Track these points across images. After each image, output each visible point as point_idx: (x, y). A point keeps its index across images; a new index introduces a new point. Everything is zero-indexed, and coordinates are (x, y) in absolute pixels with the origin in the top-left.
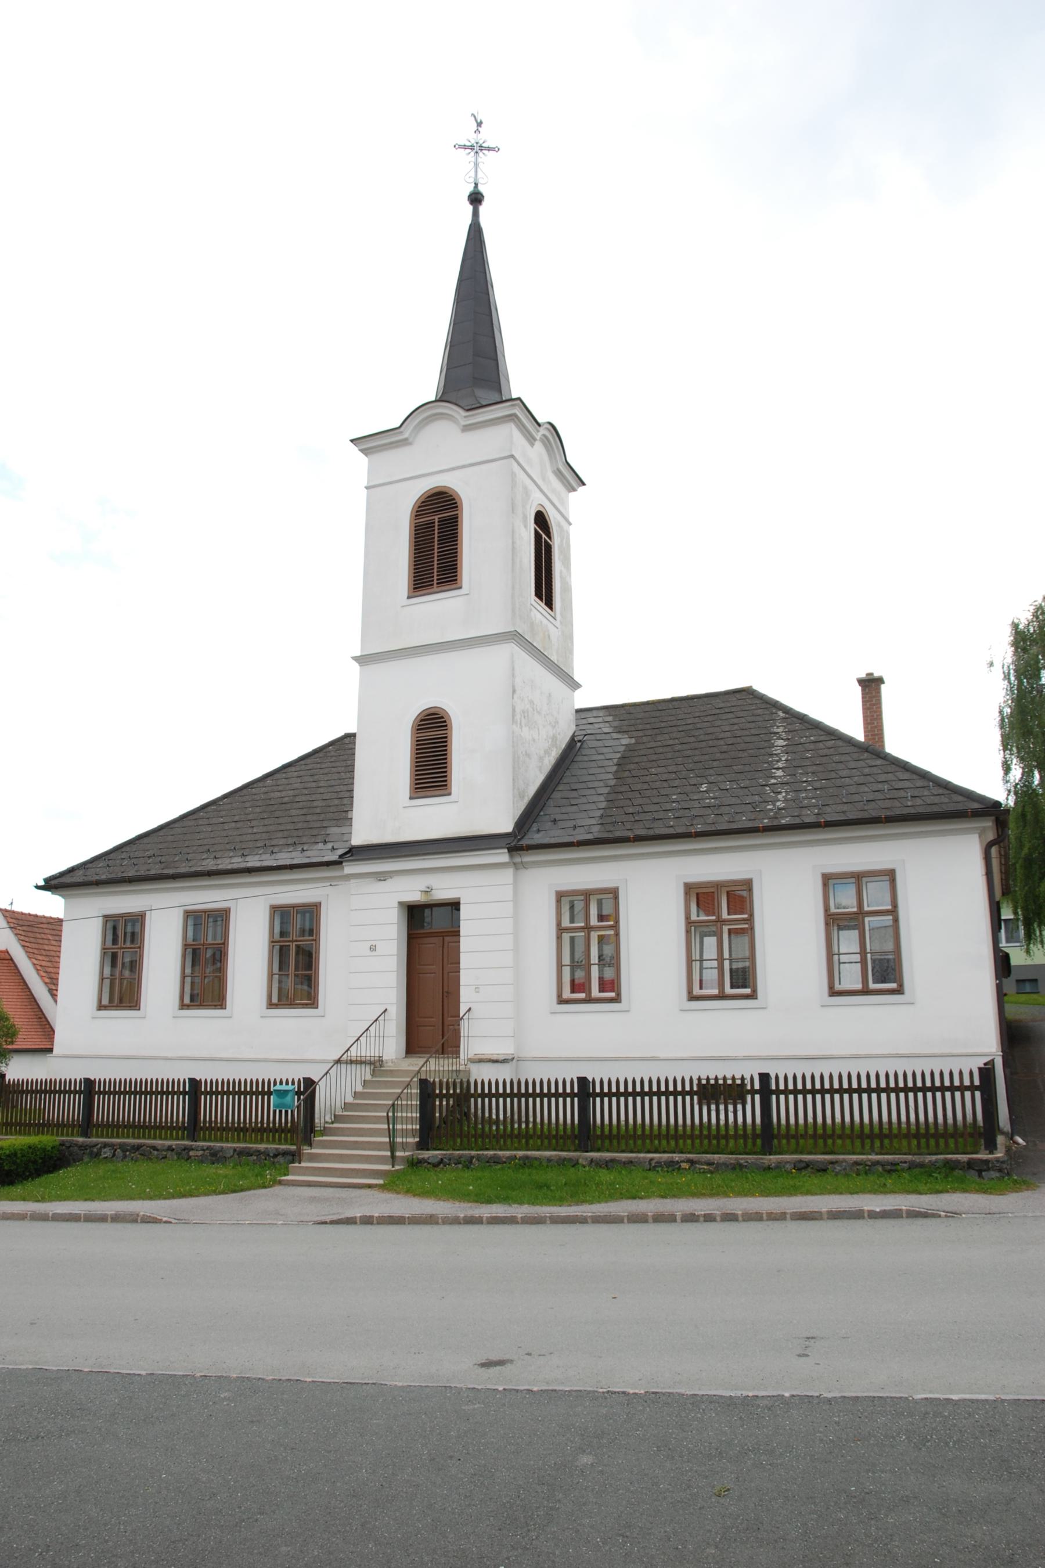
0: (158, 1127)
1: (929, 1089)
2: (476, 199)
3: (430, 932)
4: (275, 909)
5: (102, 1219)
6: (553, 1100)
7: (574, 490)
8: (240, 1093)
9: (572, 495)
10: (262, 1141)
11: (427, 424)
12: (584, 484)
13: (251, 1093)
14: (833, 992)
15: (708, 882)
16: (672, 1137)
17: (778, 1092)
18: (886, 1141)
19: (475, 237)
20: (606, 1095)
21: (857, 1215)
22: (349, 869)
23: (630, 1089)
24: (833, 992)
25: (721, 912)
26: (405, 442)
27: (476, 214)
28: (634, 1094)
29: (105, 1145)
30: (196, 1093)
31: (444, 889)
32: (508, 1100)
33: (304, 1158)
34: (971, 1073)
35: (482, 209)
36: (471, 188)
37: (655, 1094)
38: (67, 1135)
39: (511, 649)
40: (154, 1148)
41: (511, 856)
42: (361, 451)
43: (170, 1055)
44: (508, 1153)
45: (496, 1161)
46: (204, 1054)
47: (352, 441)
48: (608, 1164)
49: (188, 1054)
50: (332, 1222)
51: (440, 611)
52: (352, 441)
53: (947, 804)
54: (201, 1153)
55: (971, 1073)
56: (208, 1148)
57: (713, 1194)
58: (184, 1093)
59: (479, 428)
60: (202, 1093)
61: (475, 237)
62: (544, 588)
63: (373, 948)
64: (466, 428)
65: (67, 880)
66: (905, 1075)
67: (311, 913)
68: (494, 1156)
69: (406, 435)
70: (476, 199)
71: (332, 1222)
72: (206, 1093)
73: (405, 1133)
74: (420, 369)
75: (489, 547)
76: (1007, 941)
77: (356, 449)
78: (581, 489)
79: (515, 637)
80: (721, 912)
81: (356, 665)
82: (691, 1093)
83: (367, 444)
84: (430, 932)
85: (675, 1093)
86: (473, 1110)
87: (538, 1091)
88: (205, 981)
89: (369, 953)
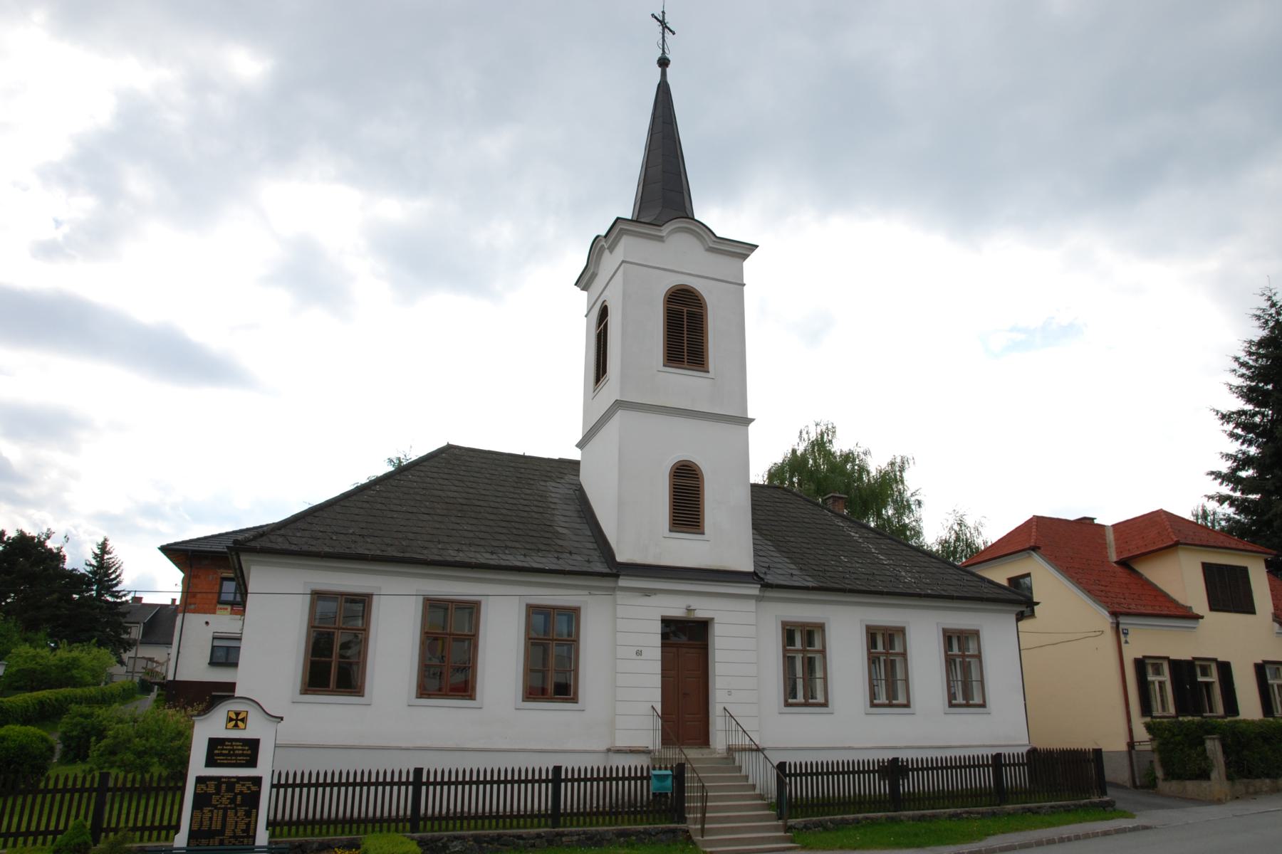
0: (595, 814)
1: (544, 781)
2: (664, 63)
3: (686, 642)
4: (532, 610)
7: (748, 256)
8: (956, 767)
10: (642, 822)
13: (965, 767)
14: (873, 705)
16: (859, 803)
17: (1005, 765)
18: (536, 820)
19: (664, 93)
21: (1087, 836)
22: (623, 582)
25: (885, 651)
27: (664, 74)
28: (947, 768)
29: (456, 838)
31: (702, 609)
34: (408, 772)
35: (668, 70)
36: (659, 54)
38: (578, 825)
39: (619, 415)
40: (520, 837)
43: (403, 745)
46: (450, 744)
48: (921, 818)
49: (428, 744)
53: (1174, 612)
54: (575, 838)
55: (408, 772)
56: (585, 833)
58: (1023, 765)
61: (664, 93)
63: (639, 653)
65: (264, 543)
66: (533, 770)
67: (363, 602)
68: (842, 820)
69: (664, 234)
70: (664, 63)
73: (694, 810)
75: (643, 332)
80: (885, 651)
82: (874, 772)
84: (686, 642)
85: (942, 768)
86: (106, 816)
88: (447, 668)
89: (634, 656)
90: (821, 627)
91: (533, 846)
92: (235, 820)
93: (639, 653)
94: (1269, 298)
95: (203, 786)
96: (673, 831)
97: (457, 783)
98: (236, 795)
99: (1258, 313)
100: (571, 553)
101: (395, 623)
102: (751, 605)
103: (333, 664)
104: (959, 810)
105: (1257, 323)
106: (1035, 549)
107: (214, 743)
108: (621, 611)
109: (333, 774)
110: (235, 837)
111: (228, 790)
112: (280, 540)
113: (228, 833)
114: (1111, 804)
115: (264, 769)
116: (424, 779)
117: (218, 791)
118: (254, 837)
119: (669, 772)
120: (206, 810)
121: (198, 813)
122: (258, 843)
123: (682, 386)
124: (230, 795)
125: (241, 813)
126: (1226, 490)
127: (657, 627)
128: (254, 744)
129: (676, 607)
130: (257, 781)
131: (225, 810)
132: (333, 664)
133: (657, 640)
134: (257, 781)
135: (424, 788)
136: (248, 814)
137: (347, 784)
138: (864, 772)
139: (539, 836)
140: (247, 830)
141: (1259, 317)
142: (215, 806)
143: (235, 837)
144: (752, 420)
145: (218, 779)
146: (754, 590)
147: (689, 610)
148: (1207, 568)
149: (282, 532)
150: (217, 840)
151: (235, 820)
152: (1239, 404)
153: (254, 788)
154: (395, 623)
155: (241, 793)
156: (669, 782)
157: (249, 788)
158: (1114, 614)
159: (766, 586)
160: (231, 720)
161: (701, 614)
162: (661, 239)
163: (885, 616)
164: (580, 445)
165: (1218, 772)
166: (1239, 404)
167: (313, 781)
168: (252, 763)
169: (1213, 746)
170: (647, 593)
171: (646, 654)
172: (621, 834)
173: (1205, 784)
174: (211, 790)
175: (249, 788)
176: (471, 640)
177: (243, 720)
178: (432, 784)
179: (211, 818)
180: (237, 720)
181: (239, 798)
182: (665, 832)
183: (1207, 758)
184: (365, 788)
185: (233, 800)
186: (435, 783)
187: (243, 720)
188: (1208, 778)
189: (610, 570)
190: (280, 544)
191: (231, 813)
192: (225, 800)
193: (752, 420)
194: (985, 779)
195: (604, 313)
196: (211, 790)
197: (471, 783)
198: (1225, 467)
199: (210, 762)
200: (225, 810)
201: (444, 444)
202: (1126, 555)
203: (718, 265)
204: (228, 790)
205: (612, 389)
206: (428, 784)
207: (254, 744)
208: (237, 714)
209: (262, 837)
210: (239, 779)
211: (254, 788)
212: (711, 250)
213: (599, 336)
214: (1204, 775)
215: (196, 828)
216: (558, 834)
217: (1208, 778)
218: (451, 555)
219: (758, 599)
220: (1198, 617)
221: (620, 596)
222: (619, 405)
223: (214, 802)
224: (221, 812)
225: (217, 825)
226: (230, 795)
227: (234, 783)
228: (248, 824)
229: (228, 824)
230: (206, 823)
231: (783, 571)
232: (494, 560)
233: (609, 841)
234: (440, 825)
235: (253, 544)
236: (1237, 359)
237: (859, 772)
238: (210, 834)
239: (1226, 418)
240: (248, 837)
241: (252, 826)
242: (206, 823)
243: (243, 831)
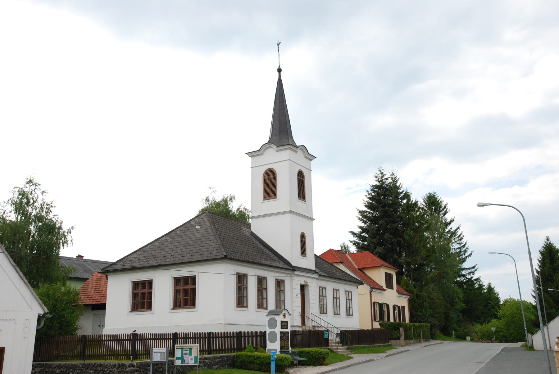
2: (279, 70)
5: (345, 367)
15: (249, 333)
19: (280, 83)
22: (296, 273)
24: (335, 314)
26: (261, 154)
50: (529, 252)
51: (272, 205)
61: (280, 83)
62: (302, 194)
64: (277, 151)
70: (279, 70)
71: (529, 252)
74: (263, 132)
75: (286, 185)
76: (287, 328)
79: (291, 212)
83: (252, 154)
99: (376, 175)
101: (163, 285)
103: (142, 299)
105: (375, 179)
108: (294, 282)
114: (390, 345)
126: (356, 239)
132: (142, 299)
141: (376, 177)
148: (386, 273)
152: (365, 209)
154: (163, 285)
158: (372, 288)
162: (296, 152)
165: (402, 338)
166: (365, 209)
169: (402, 330)
173: (398, 341)
183: (400, 333)
188: (400, 339)
189: (290, 268)
198: (358, 231)
199: (282, 328)
202: (361, 267)
212: (306, 157)
214: (399, 338)
217: (400, 339)
219: (317, 279)
220: (384, 290)
236: (368, 191)
239: (360, 212)
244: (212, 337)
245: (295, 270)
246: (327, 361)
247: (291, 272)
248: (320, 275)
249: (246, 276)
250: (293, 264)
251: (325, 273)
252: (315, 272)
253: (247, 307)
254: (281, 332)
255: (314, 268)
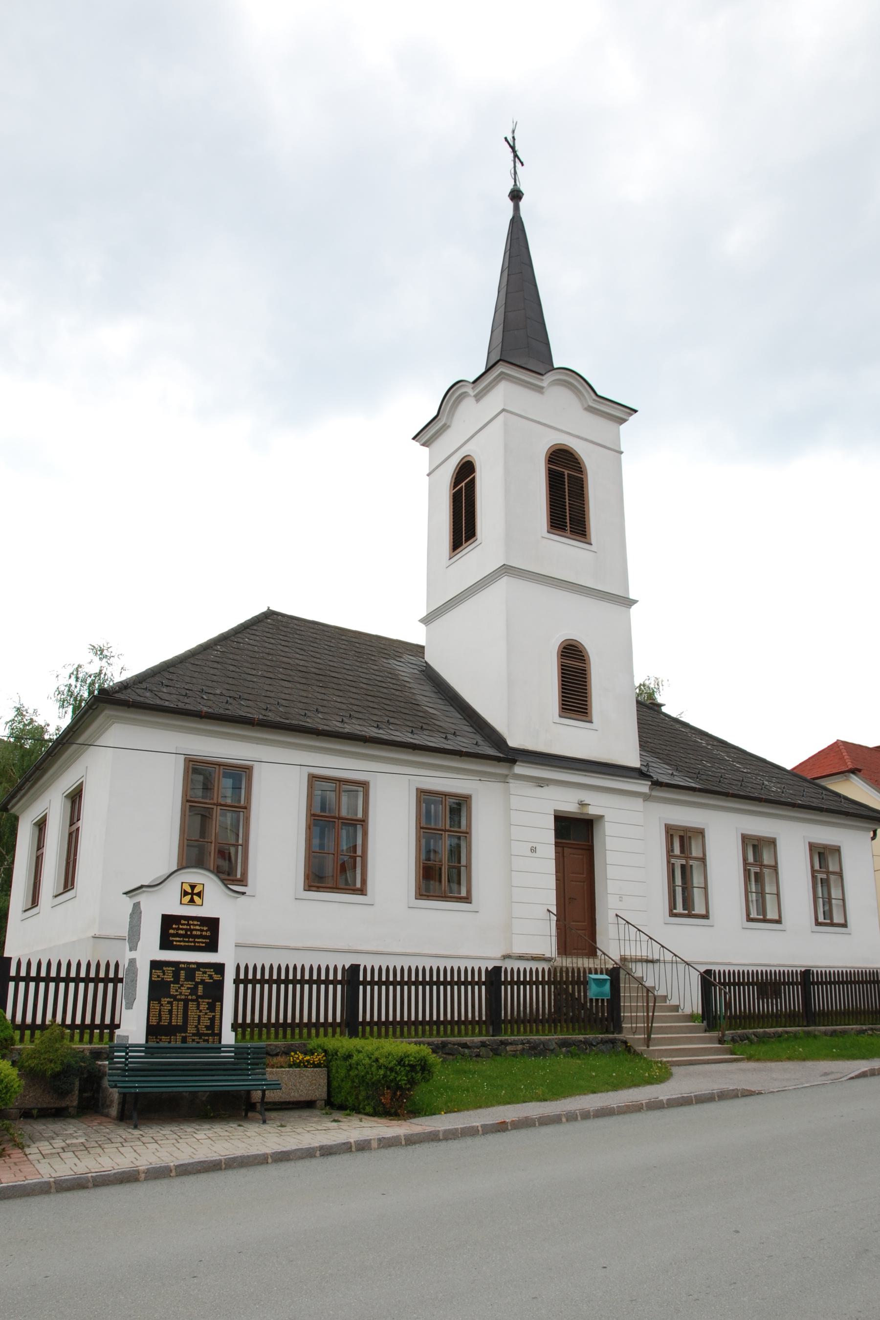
2: (516, 195)
6: (274, 986)
7: (625, 420)
8: (262, 981)
9: (623, 427)
11: (457, 405)
12: (636, 411)
19: (517, 233)
20: (332, 982)
22: (520, 769)
23: (323, 977)
27: (517, 209)
30: (805, 984)
32: (298, 986)
33: (624, 1031)
35: (522, 204)
36: (510, 186)
37: (250, 981)
40: (465, 1046)
41: (651, 789)
42: (423, 445)
44: (772, 1030)
45: (844, 1033)
47: (414, 439)
48: (833, 1033)
52: (414, 439)
54: (520, 1047)
56: (529, 1042)
57: (616, 1086)
59: (488, 391)
60: (484, 983)
61: (517, 233)
70: (516, 195)
72: (17, 979)
75: (513, 500)
77: (418, 444)
78: (634, 418)
81: (423, 626)
85: (310, 982)
87: (267, 977)
89: (530, 854)
90: (700, 833)
91: (478, 1056)
92: (197, 1014)
93: (533, 850)
94: (18, 709)
95: (159, 973)
96: (613, 1042)
97: (395, 983)
98: (197, 984)
100: (454, 734)
102: (638, 804)
104: (864, 1027)
106: (854, 771)
107: (168, 921)
108: (515, 802)
109: (29, 964)
110: (198, 1034)
111: (187, 979)
112: (148, 694)
113: (191, 1029)
115: (227, 954)
116: (13, 973)
117: (176, 979)
118: (220, 1035)
119: (605, 977)
120: (165, 1001)
121: (155, 1004)
122: (224, 1041)
123: (562, 556)
124: (190, 984)
125: (204, 1006)
127: (550, 823)
128: (213, 924)
129: (568, 801)
130: (219, 968)
131: (186, 1002)
133: (550, 836)
134: (219, 968)
135: (12, 985)
136: (212, 1008)
137: (38, 979)
138: (452, 983)
139: (483, 1044)
140: (211, 1027)
142: (174, 997)
143: (198, 1034)
144: (635, 602)
145: (175, 964)
146: (643, 787)
147: (582, 804)
149: (144, 685)
150: (179, 1037)
151: (197, 1014)
153: (217, 977)
155: (202, 982)
156: (607, 988)
157: (211, 977)
159: (657, 784)
160: (186, 893)
161: (592, 811)
162: (540, 389)
163: (760, 825)
164: (427, 620)
167: (53, 974)
168: (212, 946)
170: (541, 783)
171: (525, 849)
172: (564, 1044)
174: (169, 978)
175: (211, 977)
176: (359, 824)
177: (199, 894)
178: (33, 979)
179: (170, 1012)
180: (192, 894)
181: (200, 987)
182: (604, 1042)
184: (91, 986)
185: (194, 990)
186: (28, 979)
187: (199, 894)
189: (497, 753)
190: (149, 698)
191: (192, 1006)
192: (185, 991)
193: (635, 602)
194: (792, 999)
195: (466, 471)
196: (169, 978)
197: (48, 980)
199: (166, 944)
200: (186, 1002)
201: (265, 609)
203: (595, 427)
204: (187, 979)
205: (481, 557)
206: (365, 983)
207: (213, 924)
208: (193, 887)
209: (228, 1037)
210: (200, 965)
211: (217, 977)
212: (590, 409)
213: (456, 499)
215: (154, 1022)
216: (502, 1043)
218: (335, 725)
219: (646, 798)
221: (515, 786)
222: (506, 570)
223: (173, 992)
224: (181, 1004)
225: (177, 1021)
226: (190, 984)
227: (194, 970)
228: (212, 1020)
229: (190, 1019)
230: (165, 1016)
231: (662, 772)
232: (382, 734)
233: (552, 1051)
234: (452, 1030)
235: (118, 696)
237: (431, 983)
238: (170, 1030)
240: (213, 1034)
241: (217, 1022)
242: (165, 1016)
243: (207, 1027)
244: (813, 983)
245: (513, 762)
246: (420, 1093)
247: (501, 769)
248: (656, 784)
249: (241, 775)
250: (512, 743)
251: (697, 776)
252: (640, 774)
253: (362, 891)
254: (155, 965)
255: (633, 760)
